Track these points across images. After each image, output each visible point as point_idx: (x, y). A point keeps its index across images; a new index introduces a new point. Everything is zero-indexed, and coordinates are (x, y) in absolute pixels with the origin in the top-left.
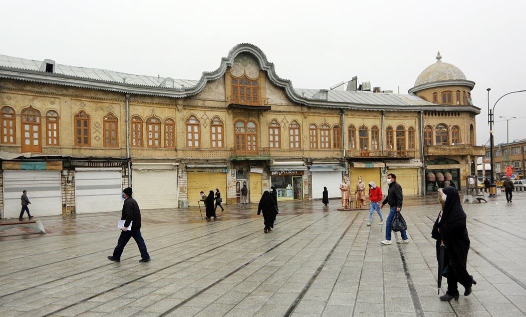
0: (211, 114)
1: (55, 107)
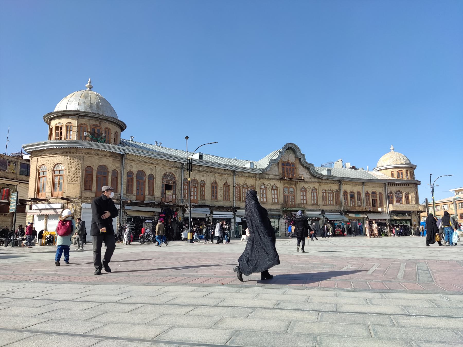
0: (272, 183)
1: (204, 178)
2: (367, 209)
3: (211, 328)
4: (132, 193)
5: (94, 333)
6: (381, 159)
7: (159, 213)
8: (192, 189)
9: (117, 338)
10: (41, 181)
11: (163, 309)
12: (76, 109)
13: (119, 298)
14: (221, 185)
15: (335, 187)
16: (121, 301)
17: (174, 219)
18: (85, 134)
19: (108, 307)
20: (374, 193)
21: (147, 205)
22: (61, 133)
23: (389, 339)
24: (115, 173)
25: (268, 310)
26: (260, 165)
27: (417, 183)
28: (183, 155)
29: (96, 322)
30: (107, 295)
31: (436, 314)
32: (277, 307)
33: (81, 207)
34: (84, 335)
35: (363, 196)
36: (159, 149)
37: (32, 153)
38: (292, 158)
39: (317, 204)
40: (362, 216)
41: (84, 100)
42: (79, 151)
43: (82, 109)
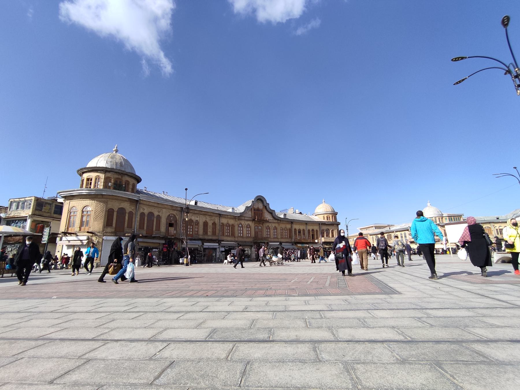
0: (247, 223)
1: (198, 219)
2: (309, 241)
3: (196, 328)
4: (143, 229)
5: (102, 337)
6: (317, 208)
7: (164, 244)
8: (189, 227)
9: (120, 340)
10: (72, 219)
11: (160, 316)
12: (104, 166)
13: (126, 308)
14: (210, 224)
15: (289, 226)
16: (128, 311)
17: (174, 249)
18: (110, 184)
19: (116, 316)
20: (313, 230)
21: (154, 238)
22: (91, 183)
23: (318, 328)
24: (131, 213)
25: (239, 313)
26: (239, 210)
27: (338, 224)
28: (183, 201)
29: (104, 328)
30: (117, 306)
31: (348, 309)
32: (245, 310)
33: (103, 239)
34: (93, 340)
35: (306, 233)
36: (165, 197)
37: (66, 198)
38: (260, 206)
39: (277, 238)
40: (305, 245)
41: (111, 160)
42: (104, 196)
43: (109, 166)
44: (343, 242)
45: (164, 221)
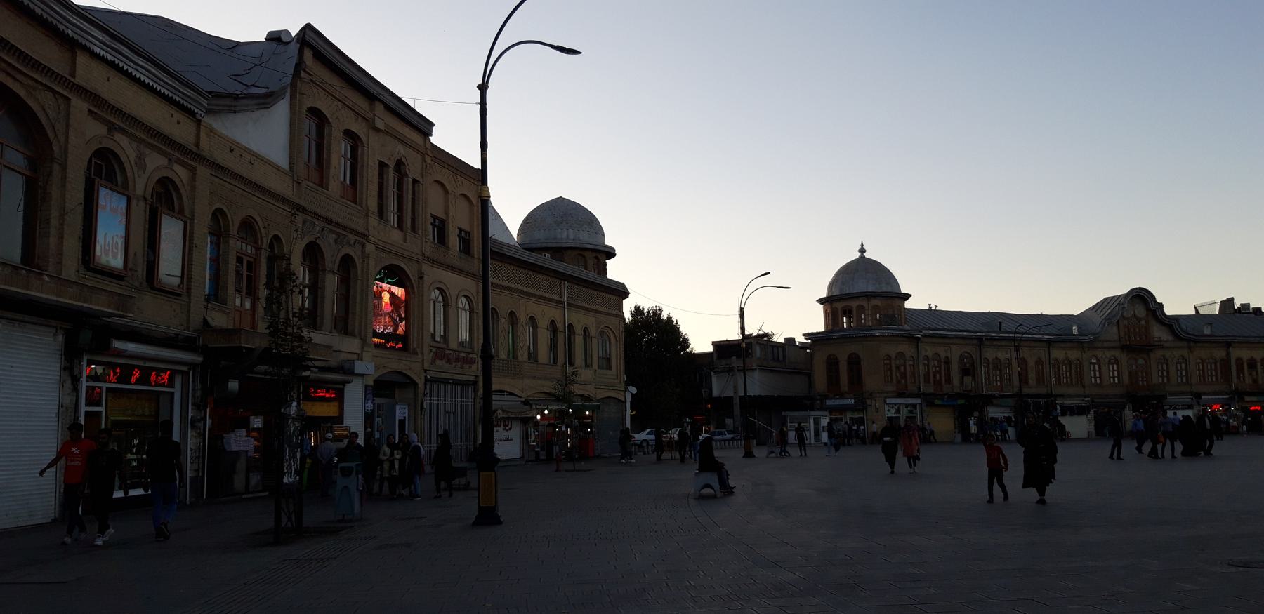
0: (1109, 354)
15: (1220, 353)
44: (628, 316)
45: (955, 366)
